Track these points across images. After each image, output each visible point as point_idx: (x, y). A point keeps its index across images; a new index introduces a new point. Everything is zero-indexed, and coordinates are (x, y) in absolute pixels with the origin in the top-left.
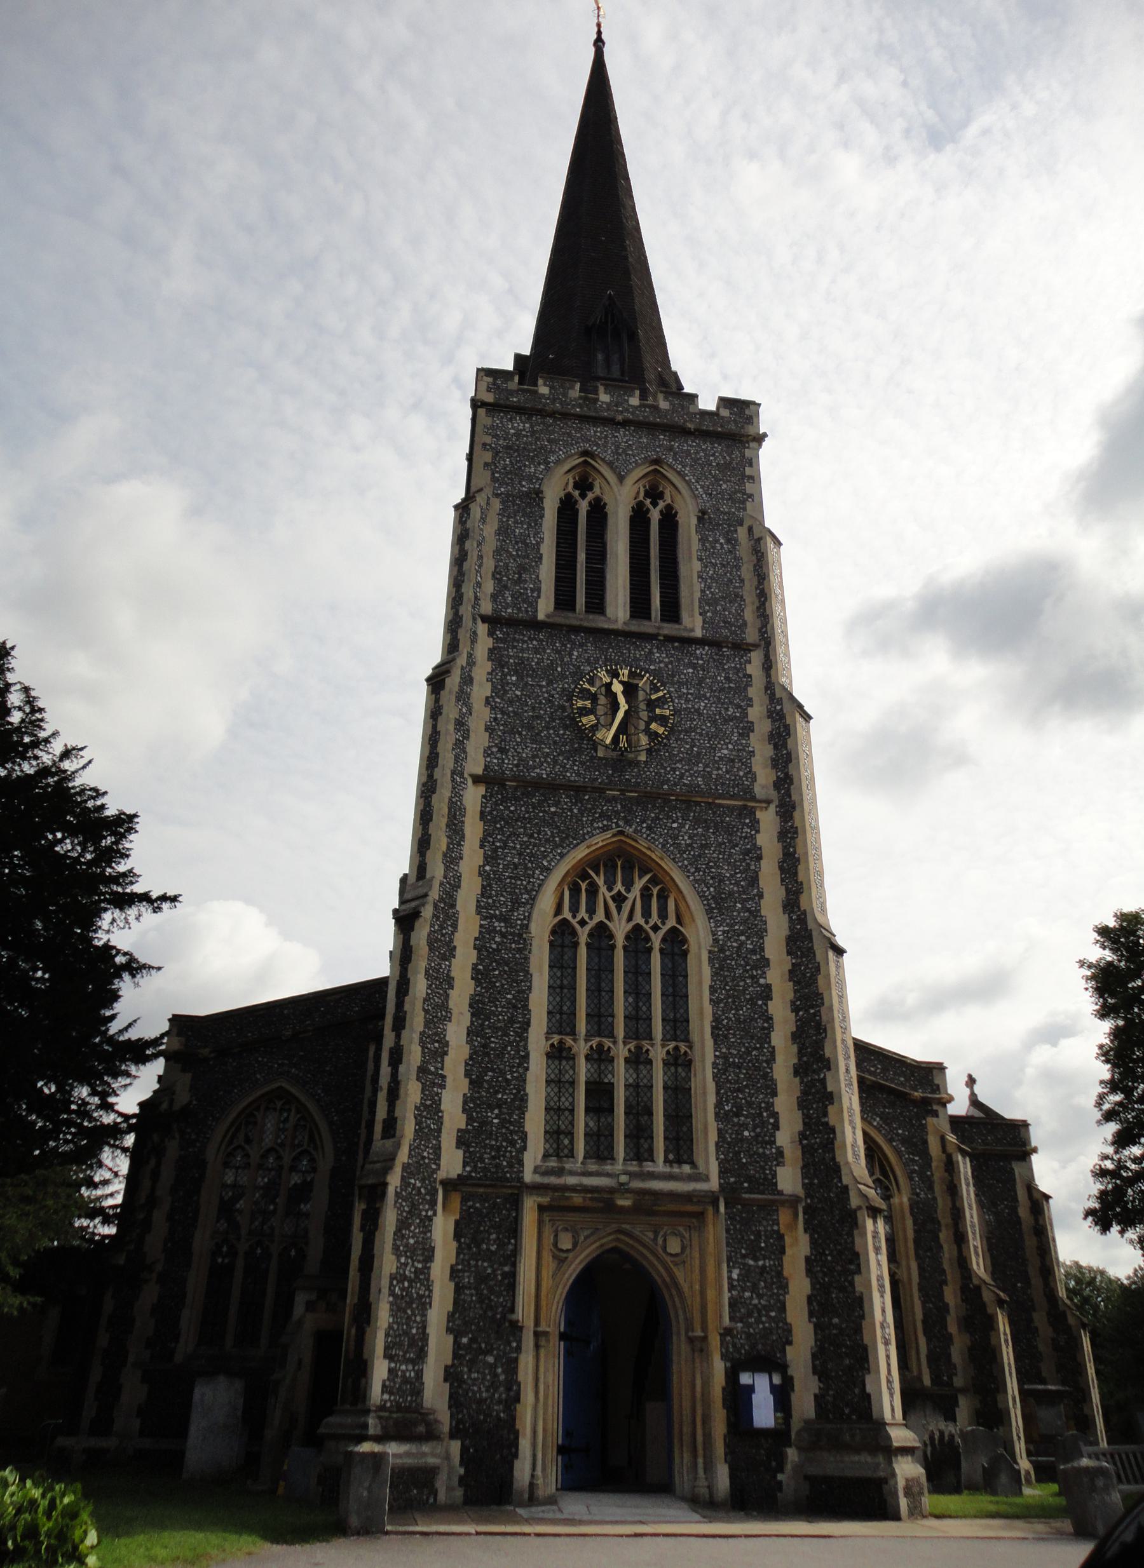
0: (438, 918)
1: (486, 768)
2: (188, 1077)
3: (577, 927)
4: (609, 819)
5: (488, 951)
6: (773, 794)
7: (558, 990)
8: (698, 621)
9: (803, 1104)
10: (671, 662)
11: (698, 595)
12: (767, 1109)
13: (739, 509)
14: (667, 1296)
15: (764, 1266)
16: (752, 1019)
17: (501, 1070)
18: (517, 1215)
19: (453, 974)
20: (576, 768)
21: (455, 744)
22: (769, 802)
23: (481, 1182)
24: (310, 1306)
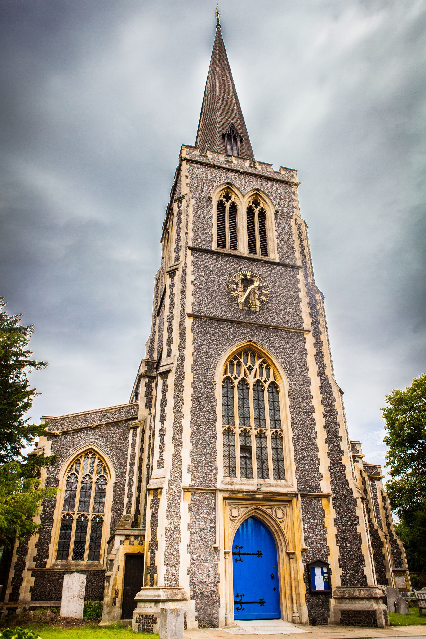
0: (177, 373)
1: (193, 311)
2: (50, 443)
3: (233, 379)
4: (245, 335)
5: (197, 389)
6: (311, 328)
7: (226, 407)
8: (277, 256)
9: (330, 455)
10: (267, 272)
11: (276, 245)
12: (315, 457)
13: (291, 212)
14: (276, 536)
15: (317, 523)
16: (307, 420)
17: (205, 440)
18: (215, 502)
19: (184, 398)
20: (231, 313)
21: (181, 300)
22: (309, 331)
23: (199, 488)
24: (122, 542)
